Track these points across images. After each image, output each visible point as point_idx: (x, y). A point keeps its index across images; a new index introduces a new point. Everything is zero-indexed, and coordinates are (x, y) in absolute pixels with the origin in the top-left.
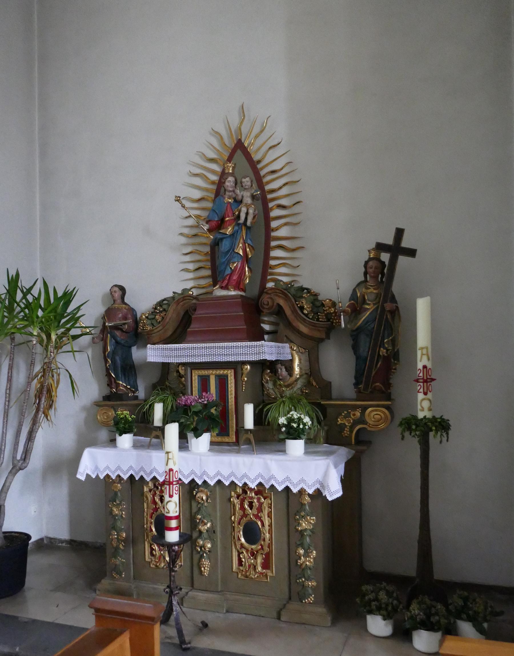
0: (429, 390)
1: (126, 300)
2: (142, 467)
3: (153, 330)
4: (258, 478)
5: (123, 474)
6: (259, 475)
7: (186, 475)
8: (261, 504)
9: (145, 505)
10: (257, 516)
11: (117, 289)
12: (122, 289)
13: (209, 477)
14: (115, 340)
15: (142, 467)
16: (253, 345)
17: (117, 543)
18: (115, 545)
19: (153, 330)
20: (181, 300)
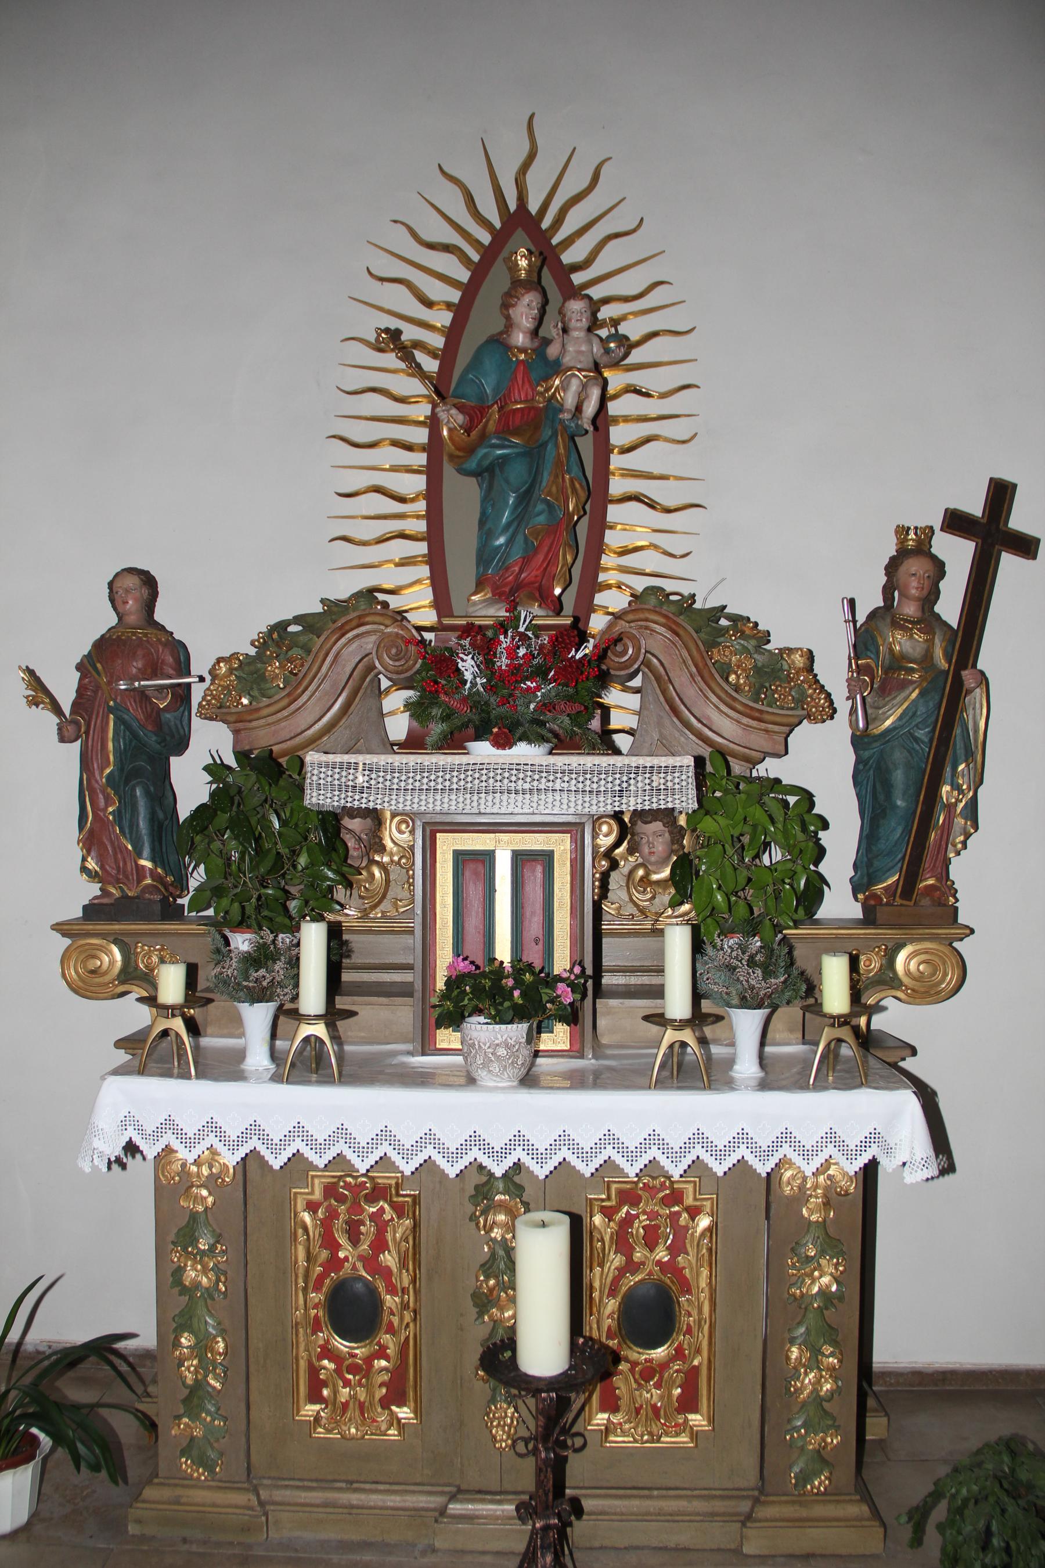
0: (633, 883)
1: (159, 616)
2: (342, 1128)
3: (258, 710)
4: (512, 1147)
5: (863, 1153)
6: (473, 1139)
7: (363, 1144)
8: (382, 1227)
9: (669, 1242)
10: (371, 1262)
11: (132, 581)
12: (149, 581)
13: (535, 1152)
14: (131, 733)
15: (342, 1128)
16: (678, 764)
17: (196, 1372)
18: (190, 1378)
19: (258, 710)
20: (354, 623)
